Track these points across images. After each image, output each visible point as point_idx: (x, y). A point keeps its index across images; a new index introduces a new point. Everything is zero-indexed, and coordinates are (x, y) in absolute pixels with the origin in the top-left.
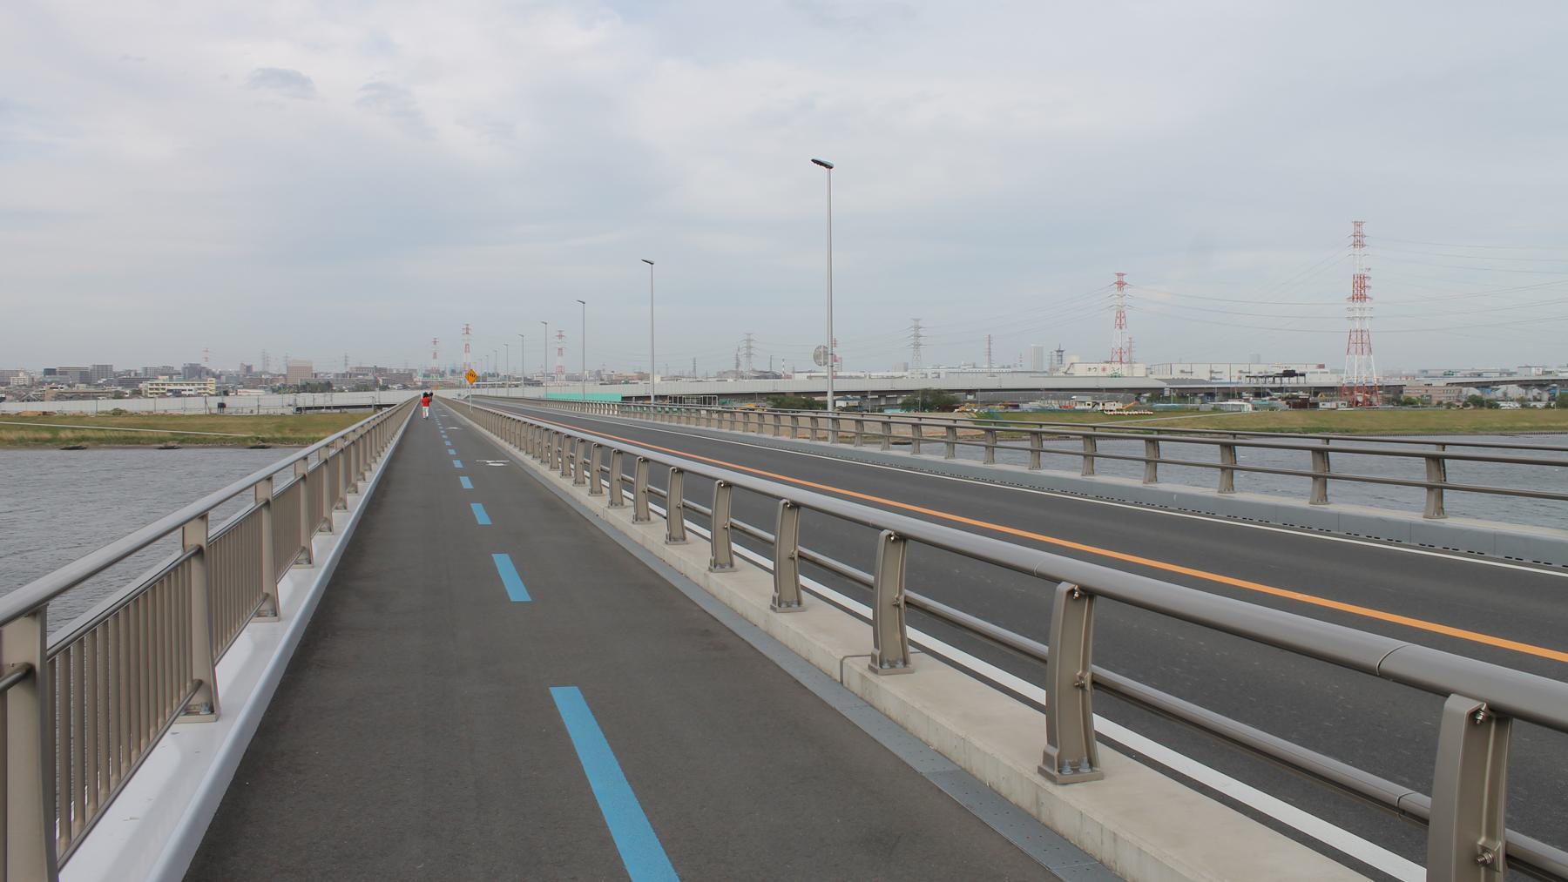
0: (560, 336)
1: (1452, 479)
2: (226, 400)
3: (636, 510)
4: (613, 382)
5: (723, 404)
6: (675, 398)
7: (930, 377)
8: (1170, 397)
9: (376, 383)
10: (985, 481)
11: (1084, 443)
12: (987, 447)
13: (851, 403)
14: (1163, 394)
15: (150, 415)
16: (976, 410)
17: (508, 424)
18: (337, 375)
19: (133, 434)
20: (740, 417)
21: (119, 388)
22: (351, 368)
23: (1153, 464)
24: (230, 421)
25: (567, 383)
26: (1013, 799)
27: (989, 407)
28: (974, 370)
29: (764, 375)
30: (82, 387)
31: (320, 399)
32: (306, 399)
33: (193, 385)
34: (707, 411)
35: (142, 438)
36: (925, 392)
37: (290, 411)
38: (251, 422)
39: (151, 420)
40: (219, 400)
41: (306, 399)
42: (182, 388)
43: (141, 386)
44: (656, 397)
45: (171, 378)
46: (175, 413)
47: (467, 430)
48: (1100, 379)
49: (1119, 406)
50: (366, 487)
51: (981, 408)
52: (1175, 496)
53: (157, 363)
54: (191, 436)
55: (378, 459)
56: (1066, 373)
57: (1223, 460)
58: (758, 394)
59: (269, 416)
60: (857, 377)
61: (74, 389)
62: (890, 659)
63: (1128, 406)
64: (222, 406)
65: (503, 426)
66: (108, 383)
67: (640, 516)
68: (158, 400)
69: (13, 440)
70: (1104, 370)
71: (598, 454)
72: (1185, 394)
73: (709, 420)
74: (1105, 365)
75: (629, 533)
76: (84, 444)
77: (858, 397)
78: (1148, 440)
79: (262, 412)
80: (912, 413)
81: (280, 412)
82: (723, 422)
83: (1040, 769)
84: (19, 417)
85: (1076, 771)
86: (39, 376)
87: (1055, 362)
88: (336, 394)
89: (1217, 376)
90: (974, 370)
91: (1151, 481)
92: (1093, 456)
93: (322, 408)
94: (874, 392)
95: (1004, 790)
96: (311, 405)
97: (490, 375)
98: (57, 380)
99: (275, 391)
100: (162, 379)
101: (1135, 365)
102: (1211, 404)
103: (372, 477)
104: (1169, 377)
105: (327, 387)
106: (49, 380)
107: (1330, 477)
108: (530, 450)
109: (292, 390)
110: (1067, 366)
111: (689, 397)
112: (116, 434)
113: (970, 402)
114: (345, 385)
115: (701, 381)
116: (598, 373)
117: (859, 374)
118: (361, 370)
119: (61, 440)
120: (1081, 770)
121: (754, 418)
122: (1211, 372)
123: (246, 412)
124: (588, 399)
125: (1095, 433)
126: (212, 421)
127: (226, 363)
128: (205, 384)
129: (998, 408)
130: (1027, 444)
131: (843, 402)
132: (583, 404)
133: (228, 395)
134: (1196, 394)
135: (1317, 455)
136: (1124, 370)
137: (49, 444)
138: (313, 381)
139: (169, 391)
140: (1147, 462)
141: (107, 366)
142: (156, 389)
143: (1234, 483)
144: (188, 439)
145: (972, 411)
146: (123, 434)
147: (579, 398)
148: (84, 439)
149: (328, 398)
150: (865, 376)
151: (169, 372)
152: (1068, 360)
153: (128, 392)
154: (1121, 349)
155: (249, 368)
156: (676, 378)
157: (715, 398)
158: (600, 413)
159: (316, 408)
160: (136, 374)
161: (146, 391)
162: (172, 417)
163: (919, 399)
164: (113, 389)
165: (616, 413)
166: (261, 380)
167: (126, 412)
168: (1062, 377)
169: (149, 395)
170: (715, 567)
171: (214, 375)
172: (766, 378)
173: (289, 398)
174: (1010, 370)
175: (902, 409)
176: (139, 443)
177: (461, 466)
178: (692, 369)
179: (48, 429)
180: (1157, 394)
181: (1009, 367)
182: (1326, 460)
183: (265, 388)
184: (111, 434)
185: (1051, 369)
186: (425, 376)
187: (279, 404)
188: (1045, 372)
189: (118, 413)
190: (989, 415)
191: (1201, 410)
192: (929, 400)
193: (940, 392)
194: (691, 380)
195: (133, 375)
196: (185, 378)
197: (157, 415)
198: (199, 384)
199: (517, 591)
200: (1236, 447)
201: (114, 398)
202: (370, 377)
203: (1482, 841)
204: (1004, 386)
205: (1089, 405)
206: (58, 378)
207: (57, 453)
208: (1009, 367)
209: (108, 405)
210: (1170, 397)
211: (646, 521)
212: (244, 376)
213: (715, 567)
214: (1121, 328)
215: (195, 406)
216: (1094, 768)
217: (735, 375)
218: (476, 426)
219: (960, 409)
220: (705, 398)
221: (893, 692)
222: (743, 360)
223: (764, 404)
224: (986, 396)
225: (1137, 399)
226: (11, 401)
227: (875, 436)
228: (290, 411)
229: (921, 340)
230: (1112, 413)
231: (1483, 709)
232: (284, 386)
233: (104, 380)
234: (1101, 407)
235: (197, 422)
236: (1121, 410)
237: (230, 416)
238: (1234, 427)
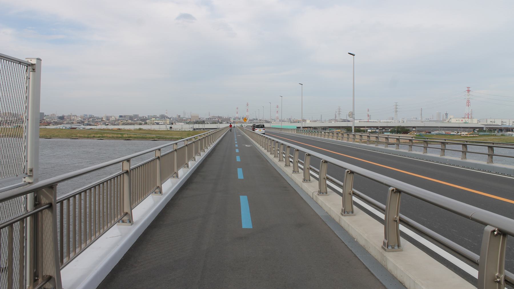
0: (277, 107)
1: (469, 150)
2: (172, 126)
3: (294, 168)
4: (294, 122)
5: (330, 130)
6: (314, 128)
7: (401, 122)
8: (486, 130)
9: (218, 121)
10: (395, 154)
11: (441, 146)
12: (409, 145)
13: (373, 131)
14: (483, 129)
15: (149, 130)
16: (415, 134)
17: (258, 137)
18: (207, 119)
19: (145, 136)
20: (335, 134)
21: (141, 122)
22: (211, 116)
23: (444, 150)
24: (173, 133)
25: (279, 122)
26: (336, 221)
27: (421, 133)
28: (416, 120)
29: (344, 121)
30: (130, 121)
31: (201, 126)
32: (197, 126)
33: (162, 121)
34: (324, 132)
35: (147, 137)
36: (398, 127)
37: (192, 130)
38: (179, 133)
39: (150, 132)
40: (170, 126)
41: (197, 126)
42: (159, 122)
43: (147, 121)
44: (303, 127)
45: (156, 119)
46: (157, 130)
47: (243, 136)
48: (460, 124)
49: (467, 133)
50: (208, 150)
51: (418, 133)
52: (448, 160)
53: (152, 114)
54: (162, 137)
55: (213, 144)
56: (448, 121)
57: (489, 152)
58: (342, 127)
59: (185, 131)
60: (376, 122)
61: (128, 122)
62: (347, 211)
63: (470, 133)
64: (171, 128)
65: (258, 138)
66: (137, 120)
67: (306, 179)
68: (152, 126)
69: (110, 137)
70: (462, 120)
71: (282, 147)
72: (492, 130)
73: (325, 135)
74: (463, 119)
75: (267, 154)
76: (130, 139)
77: (376, 128)
78: (489, 147)
79: (183, 130)
80: (394, 134)
81: (188, 130)
82: (322, 135)
83: (382, 247)
84: (112, 130)
85: (393, 248)
86: (118, 118)
87: (445, 118)
88: (205, 125)
89: (504, 123)
90: (416, 120)
91: (442, 155)
92: (427, 147)
93: (202, 129)
94: (380, 127)
95: (335, 219)
96: (198, 128)
97: (254, 119)
98: (123, 119)
99: (187, 123)
100: (153, 119)
101: (474, 119)
102: (501, 133)
103: (210, 148)
104: (486, 123)
105: (203, 122)
106: (121, 119)
107: (467, 152)
108: (266, 148)
109: (192, 123)
110: (449, 119)
111: (319, 127)
112: (140, 136)
113: (414, 131)
114: (209, 122)
115: (323, 122)
116: (290, 119)
117: (376, 121)
118: (214, 117)
119: (124, 137)
120: (395, 248)
121: (340, 135)
122: (502, 122)
123: (178, 130)
124: (283, 127)
125: (493, 145)
126: (168, 132)
127: (173, 114)
128: (166, 121)
129: (423, 133)
130: (423, 145)
131: (370, 130)
132: (281, 129)
133: (173, 124)
134: (495, 130)
135: (489, 148)
136: (469, 121)
137: (120, 138)
138: (199, 120)
139: (155, 123)
140: (463, 152)
141: (137, 115)
142: (152, 122)
143: (466, 156)
144: (161, 138)
145: (414, 134)
146: (142, 136)
147: (280, 127)
148: (130, 137)
149: (203, 126)
150: (378, 122)
151: (155, 117)
152: (449, 117)
153: (143, 123)
154: (468, 113)
155: (179, 116)
156: (315, 121)
157: (327, 128)
158: (289, 132)
159: (200, 129)
160: (146, 117)
161: (148, 123)
162: (156, 131)
163: (396, 129)
164: (139, 122)
165: (295, 132)
166: (183, 120)
167: (143, 129)
168: (447, 123)
169: (149, 124)
170: (320, 193)
171: (169, 118)
172: (345, 121)
173: (191, 126)
174: (429, 120)
175: (390, 133)
176: (146, 139)
177: (237, 146)
178: (320, 118)
179: (120, 134)
180: (481, 129)
181: (429, 119)
182: (492, 150)
183: (184, 122)
184: (138, 136)
185: (443, 120)
186: (234, 119)
187: (188, 127)
188: (441, 121)
189: (140, 129)
190: (420, 135)
191: (497, 135)
192: (400, 130)
193: (404, 127)
194: (320, 122)
195: (145, 118)
196: (160, 119)
197: (151, 130)
198: (164, 121)
199: (247, 223)
200: (467, 145)
201: (139, 125)
202: (217, 119)
203: (497, 274)
204: (426, 126)
205: (456, 133)
206: (123, 118)
207: (123, 141)
208: (429, 119)
209: (137, 127)
210: (486, 130)
211: (351, 213)
212: (178, 118)
213: (320, 193)
214: (468, 106)
215: (163, 128)
216: (400, 248)
217: (335, 120)
218: (251, 139)
219: (410, 133)
220: (324, 128)
221: (321, 199)
222: (337, 115)
223: (343, 130)
224: (419, 129)
225: (474, 131)
226: (110, 125)
227: (374, 141)
228: (192, 130)
229: (398, 110)
230: (464, 136)
231: (496, 230)
232: (190, 122)
233: (137, 119)
234: (460, 134)
235: (164, 132)
236: (467, 135)
237: (173, 131)
238: (509, 142)
